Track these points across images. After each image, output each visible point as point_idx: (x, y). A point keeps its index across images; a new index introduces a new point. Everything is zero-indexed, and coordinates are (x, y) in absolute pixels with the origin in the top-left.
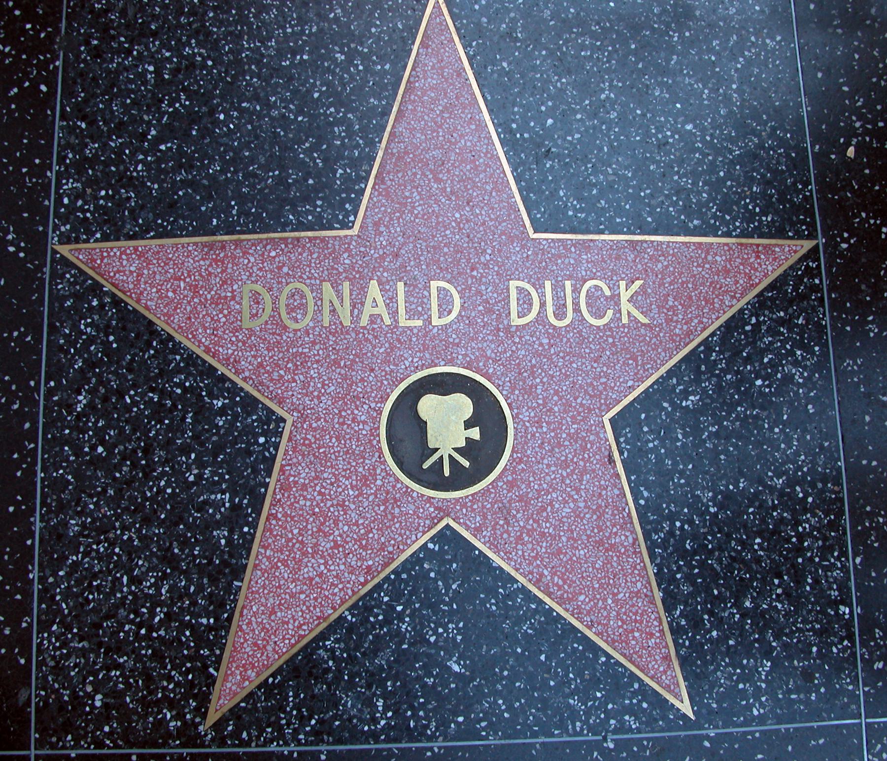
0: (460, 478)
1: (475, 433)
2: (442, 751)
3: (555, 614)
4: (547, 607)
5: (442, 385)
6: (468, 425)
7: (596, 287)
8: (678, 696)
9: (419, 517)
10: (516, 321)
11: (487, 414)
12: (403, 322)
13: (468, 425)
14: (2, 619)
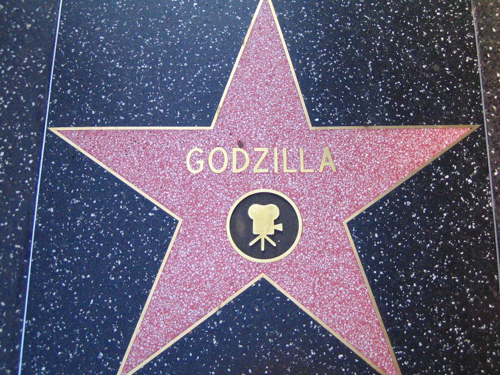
0: (271, 252)
1: (280, 227)
2: (359, 248)
3: (424, 123)
4: (330, 335)
5: (264, 199)
6: (276, 222)
7: (219, 152)
9: (251, 271)
11: (287, 216)
13: (276, 222)
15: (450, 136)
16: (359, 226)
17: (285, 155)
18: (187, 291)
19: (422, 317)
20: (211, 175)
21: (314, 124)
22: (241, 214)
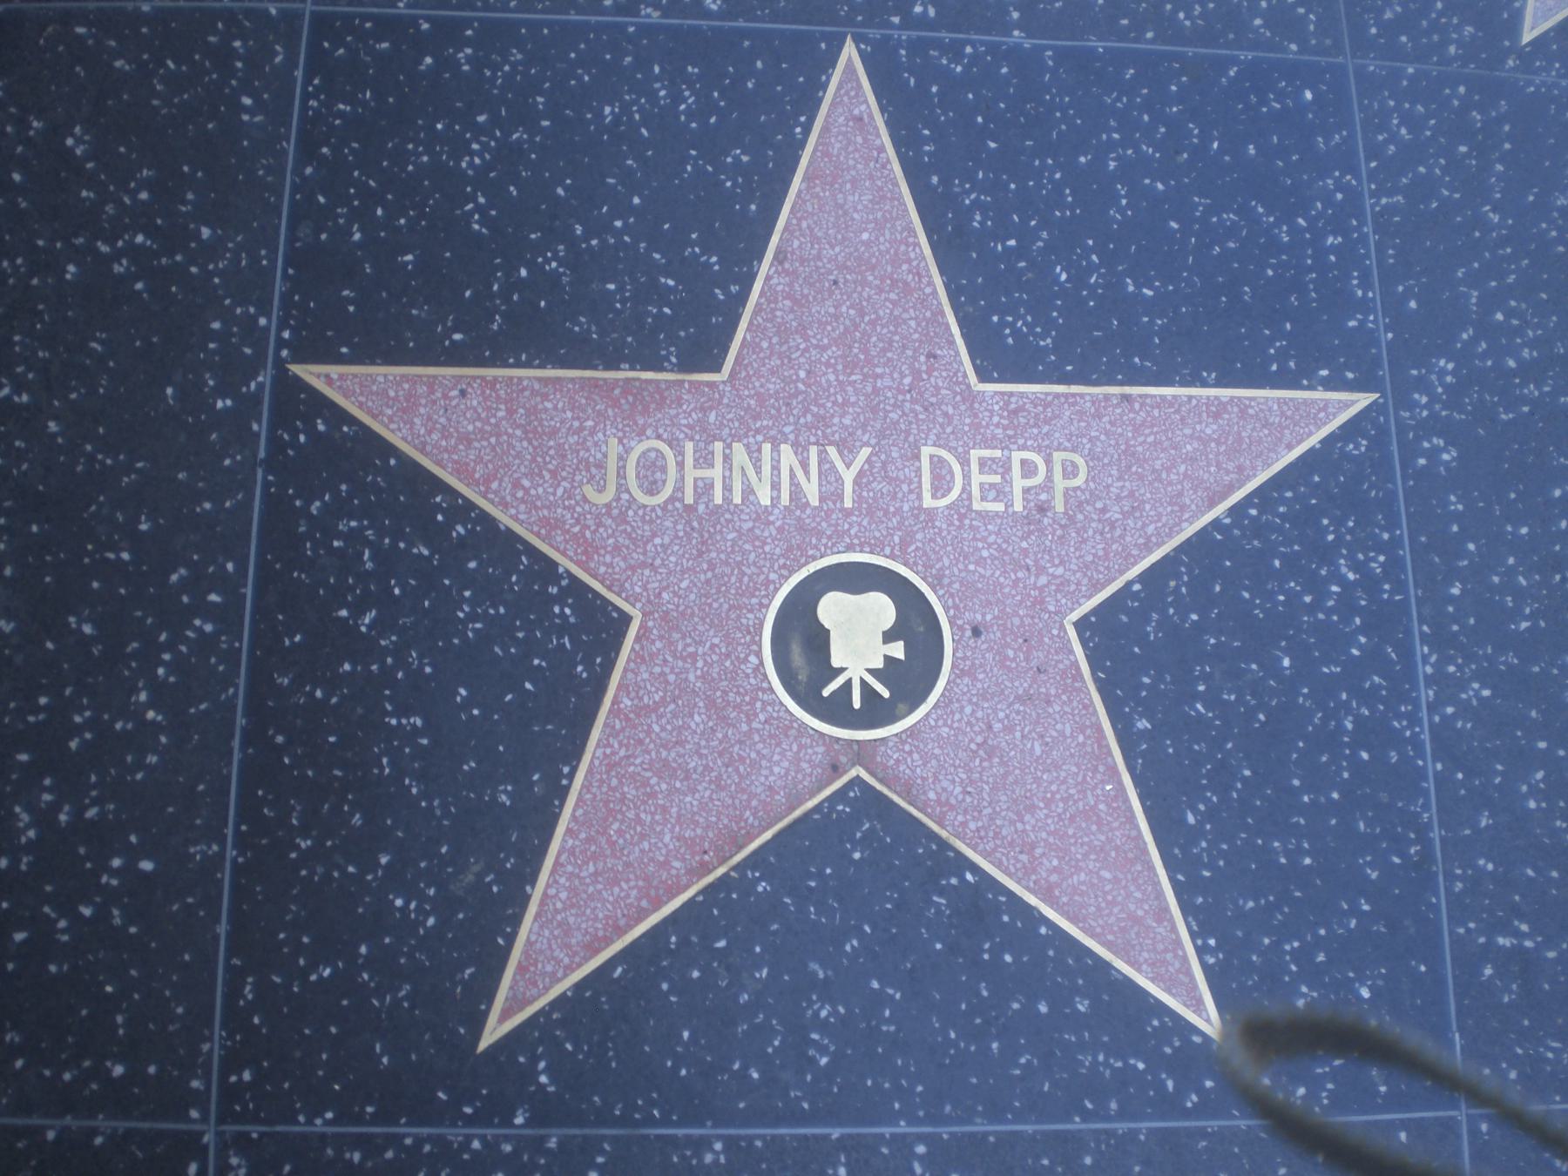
0: (876, 712)
1: (898, 650)
6: (889, 637)
7: (651, 492)
9: (787, 765)
10: (928, 502)
11: (915, 623)
13: (889, 637)
14: (7, 627)
19: (1119, 99)
20: (1038, 450)
22: (803, 636)
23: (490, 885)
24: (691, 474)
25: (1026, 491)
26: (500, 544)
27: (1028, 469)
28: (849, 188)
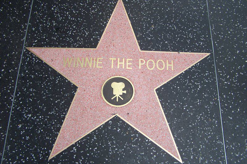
0: (121, 102)
1: (125, 92)
5: (118, 80)
6: (123, 90)
7: (151, 61)
8: (178, 158)
9: (105, 113)
11: (128, 87)
12: (97, 67)
13: (123, 90)
15: (36, 51)
16: (75, 88)
17: (75, 64)
18: (77, 125)
21: (142, 49)
22: (108, 91)
23: (159, 17)
24: (168, 65)
25: (141, 65)
26: (55, 73)
27: (142, 62)
28: (119, 22)
